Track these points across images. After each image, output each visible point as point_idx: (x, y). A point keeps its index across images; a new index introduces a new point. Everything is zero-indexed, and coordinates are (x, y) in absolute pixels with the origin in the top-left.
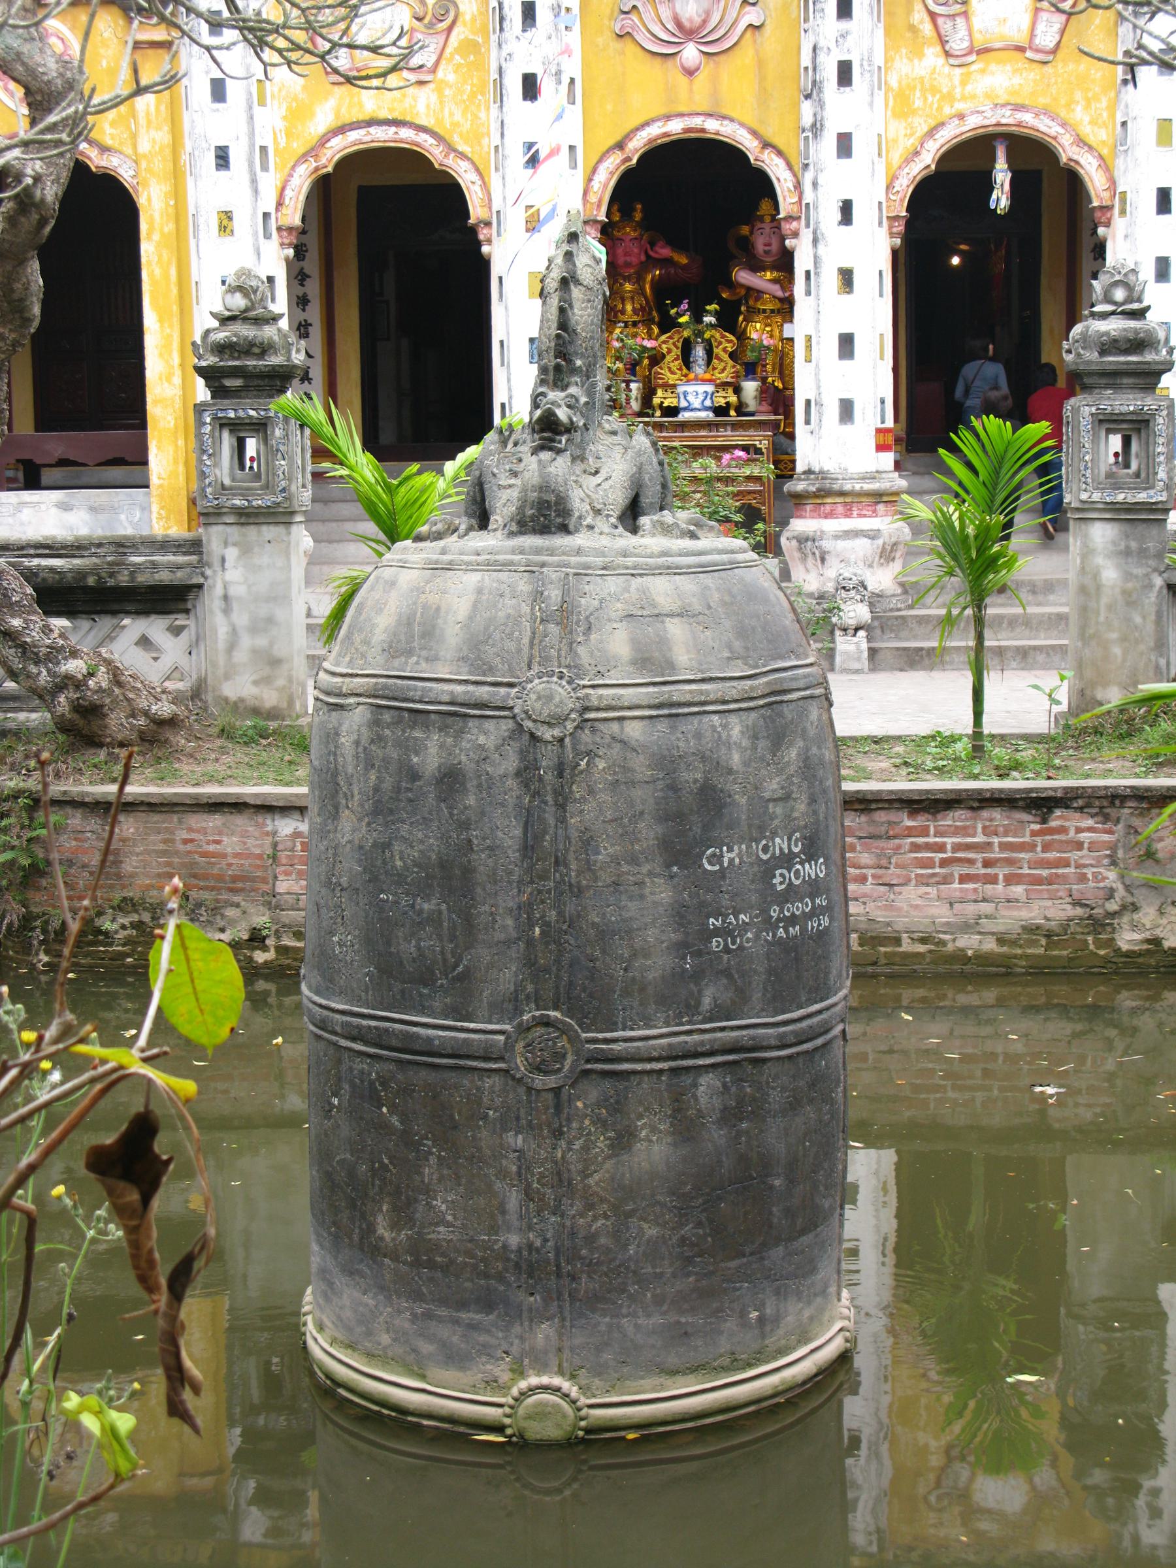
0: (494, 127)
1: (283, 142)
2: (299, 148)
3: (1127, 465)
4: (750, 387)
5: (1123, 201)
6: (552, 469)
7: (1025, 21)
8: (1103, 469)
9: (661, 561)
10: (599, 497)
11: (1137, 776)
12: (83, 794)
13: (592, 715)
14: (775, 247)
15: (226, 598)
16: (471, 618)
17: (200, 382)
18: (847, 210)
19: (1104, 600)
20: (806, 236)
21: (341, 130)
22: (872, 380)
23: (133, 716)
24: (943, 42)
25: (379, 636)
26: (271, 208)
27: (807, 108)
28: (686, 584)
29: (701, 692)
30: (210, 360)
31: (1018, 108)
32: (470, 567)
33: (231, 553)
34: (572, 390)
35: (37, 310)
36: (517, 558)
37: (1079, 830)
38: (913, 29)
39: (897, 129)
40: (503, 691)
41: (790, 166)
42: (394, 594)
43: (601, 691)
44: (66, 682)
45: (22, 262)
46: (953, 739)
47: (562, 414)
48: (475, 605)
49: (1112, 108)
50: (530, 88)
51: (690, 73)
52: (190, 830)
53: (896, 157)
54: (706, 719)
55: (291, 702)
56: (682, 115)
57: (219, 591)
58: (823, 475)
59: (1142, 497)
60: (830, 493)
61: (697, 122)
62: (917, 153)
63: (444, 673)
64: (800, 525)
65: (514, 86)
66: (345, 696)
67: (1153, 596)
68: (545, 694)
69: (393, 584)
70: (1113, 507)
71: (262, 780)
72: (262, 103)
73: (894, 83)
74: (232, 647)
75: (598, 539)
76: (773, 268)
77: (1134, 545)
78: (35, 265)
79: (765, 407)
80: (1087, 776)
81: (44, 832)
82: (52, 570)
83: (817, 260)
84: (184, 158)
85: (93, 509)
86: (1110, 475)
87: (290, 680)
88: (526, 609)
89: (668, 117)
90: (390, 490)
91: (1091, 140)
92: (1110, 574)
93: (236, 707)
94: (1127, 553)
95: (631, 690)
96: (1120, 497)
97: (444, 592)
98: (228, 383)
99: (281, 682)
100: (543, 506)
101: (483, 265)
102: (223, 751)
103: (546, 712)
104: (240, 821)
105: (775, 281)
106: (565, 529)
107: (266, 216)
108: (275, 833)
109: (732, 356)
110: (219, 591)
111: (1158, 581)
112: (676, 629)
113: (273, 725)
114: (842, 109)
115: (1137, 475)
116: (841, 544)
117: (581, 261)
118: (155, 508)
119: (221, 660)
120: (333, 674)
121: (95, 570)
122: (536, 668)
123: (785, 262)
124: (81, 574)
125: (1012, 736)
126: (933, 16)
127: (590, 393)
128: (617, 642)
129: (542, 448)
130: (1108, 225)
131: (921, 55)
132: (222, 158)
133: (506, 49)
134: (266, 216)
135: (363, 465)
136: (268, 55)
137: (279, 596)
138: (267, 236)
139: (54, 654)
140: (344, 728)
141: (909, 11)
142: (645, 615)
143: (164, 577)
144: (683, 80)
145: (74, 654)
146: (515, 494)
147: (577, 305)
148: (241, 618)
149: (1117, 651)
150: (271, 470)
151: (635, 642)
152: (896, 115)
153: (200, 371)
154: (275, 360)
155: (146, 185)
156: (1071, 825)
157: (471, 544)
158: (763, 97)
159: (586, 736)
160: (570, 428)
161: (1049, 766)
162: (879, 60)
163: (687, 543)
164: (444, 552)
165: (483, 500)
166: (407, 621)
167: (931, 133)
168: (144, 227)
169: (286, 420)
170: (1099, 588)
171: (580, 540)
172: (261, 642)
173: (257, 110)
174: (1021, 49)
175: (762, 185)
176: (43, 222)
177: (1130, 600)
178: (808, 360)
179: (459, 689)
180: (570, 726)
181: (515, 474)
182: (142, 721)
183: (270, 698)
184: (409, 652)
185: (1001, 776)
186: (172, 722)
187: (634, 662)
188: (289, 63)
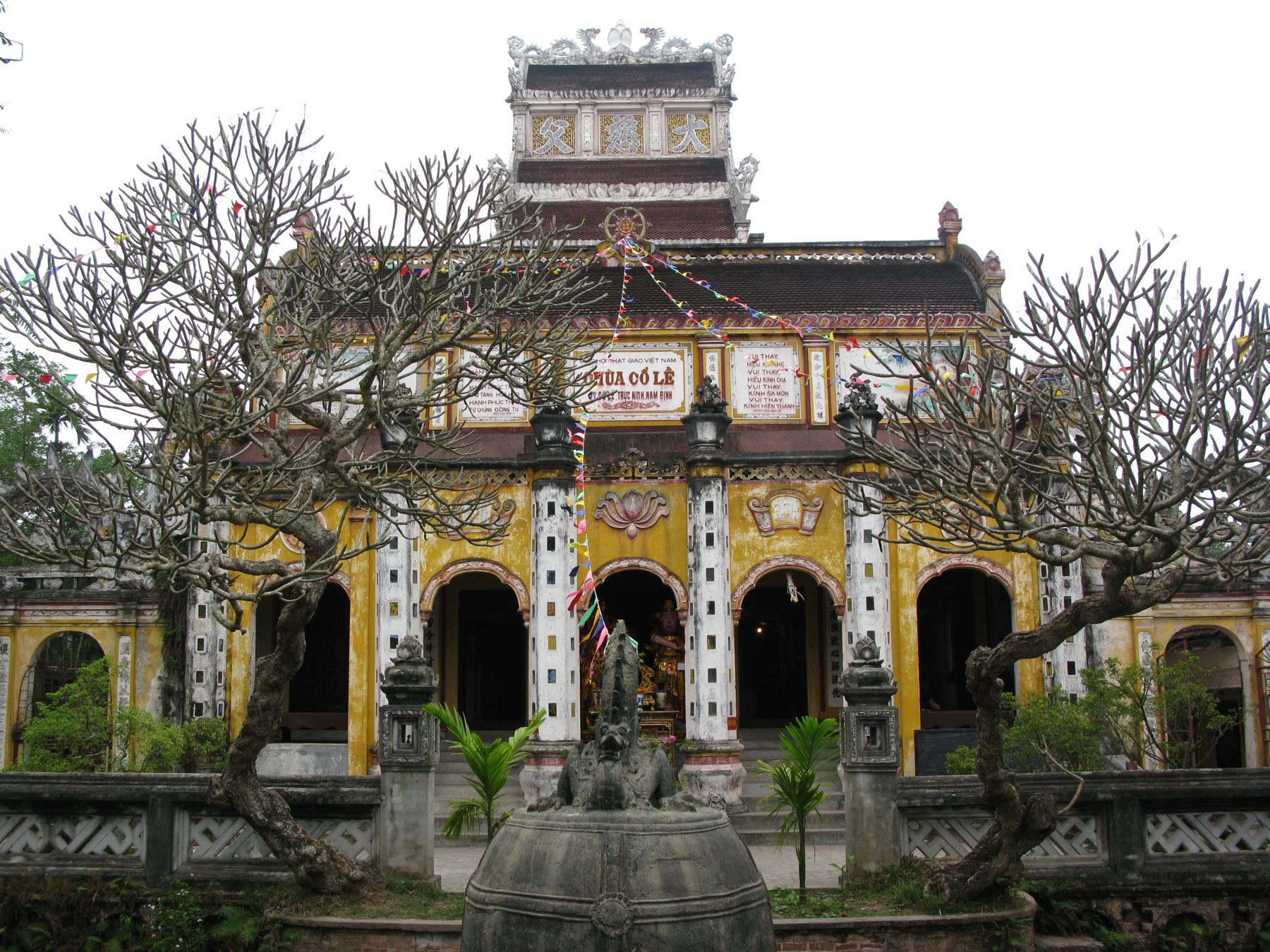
0: (532, 563)
1: (425, 568)
2: (432, 571)
3: (874, 743)
4: (661, 695)
5: (850, 603)
6: (612, 771)
7: (798, 515)
8: (863, 745)
9: (676, 826)
10: (638, 786)
11: (891, 914)
12: (310, 922)
13: (639, 921)
14: (673, 623)
15: (392, 812)
16: (565, 861)
17: (383, 695)
18: (711, 607)
19: (866, 816)
20: (691, 620)
21: (455, 563)
22: (724, 693)
23: (340, 877)
24: (758, 525)
25: (508, 869)
26: (417, 601)
27: (691, 556)
28: (691, 840)
29: (702, 906)
30: (390, 684)
31: (796, 557)
32: (564, 829)
33: (396, 787)
34: (623, 724)
35: (302, 658)
36: (592, 824)
37: (862, 946)
38: (743, 518)
39: (736, 566)
40: (585, 906)
41: (682, 585)
42: (517, 843)
43: (644, 907)
44: (306, 858)
45: (297, 633)
46: (785, 893)
47: (618, 739)
48: (568, 853)
49: (842, 558)
50: (551, 544)
51: (632, 538)
52: (369, 944)
53: (736, 580)
54: (705, 922)
55: (425, 870)
56: (627, 558)
57: (388, 808)
58: (701, 741)
59: (884, 760)
60: (704, 751)
61: (636, 562)
62: (746, 579)
63: (549, 895)
64: (689, 768)
65: (543, 542)
66: (487, 904)
67: (891, 813)
68: (610, 907)
69: (516, 837)
70: (868, 766)
71: (410, 916)
72: (416, 549)
73: (734, 544)
74: (394, 839)
75: (638, 813)
76: (672, 634)
77: (880, 786)
78: (303, 634)
79: (669, 706)
80: (864, 914)
81: (289, 944)
82: (299, 794)
83: (697, 632)
84: (375, 575)
85: (318, 754)
86: (866, 748)
87: (425, 857)
88: (598, 855)
89: (620, 560)
90: (485, 753)
91: (833, 573)
92: (868, 801)
93: (396, 872)
94: (877, 790)
95: (662, 906)
96: (872, 760)
97: (549, 844)
98: (398, 696)
99: (420, 859)
100: (607, 793)
101: (525, 631)
102: (388, 897)
103: (611, 919)
104: (397, 939)
105: (673, 641)
106: (620, 807)
107: (415, 605)
108: (416, 947)
109: (652, 679)
110: (388, 808)
111: (893, 805)
112: (686, 867)
113: (415, 883)
114: (710, 557)
115: (880, 748)
116: (710, 778)
117: (627, 650)
118: (350, 754)
119: (388, 846)
120: (479, 890)
121: (322, 795)
122: (605, 892)
123: (679, 632)
124: (314, 797)
125: (819, 890)
126: (753, 512)
127: (632, 726)
128: (653, 876)
129: (606, 759)
130: (842, 615)
131: (747, 531)
132: (394, 576)
133: (540, 525)
134: (415, 605)
135: (471, 740)
136: (428, 528)
137: (421, 811)
138: (415, 615)
139: (299, 842)
140: (487, 923)
141: (741, 510)
142: (668, 860)
143: (359, 799)
144: (628, 541)
145: (310, 843)
146: (590, 785)
147: (625, 676)
148: (400, 823)
149: (873, 843)
150: (419, 743)
151: (664, 877)
152: (735, 560)
153: (383, 689)
154: (424, 684)
155: (354, 588)
156: (858, 943)
157: (564, 814)
158: (668, 550)
159: (635, 934)
160: (622, 747)
161: (843, 908)
162: (727, 533)
163: (689, 814)
164: (547, 819)
165: (569, 787)
166: (526, 861)
167: (753, 569)
168: (352, 610)
169: (428, 716)
170: (862, 809)
171: (629, 813)
172: (411, 836)
173: (413, 553)
174: (797, 529)
175: (668, 593)
176: (309, 613)
177: (879, 815)
178: (692, 682)
179: (558, 904)
180: (626, 928)
181: (588, 772)
182: (344, 881)
183: (414, 867)
184: (527, 880)
185: (818, 915)
186: (361, 881)
187: (663, 888)
188: (437, 532)
